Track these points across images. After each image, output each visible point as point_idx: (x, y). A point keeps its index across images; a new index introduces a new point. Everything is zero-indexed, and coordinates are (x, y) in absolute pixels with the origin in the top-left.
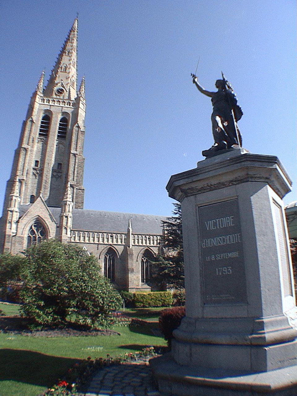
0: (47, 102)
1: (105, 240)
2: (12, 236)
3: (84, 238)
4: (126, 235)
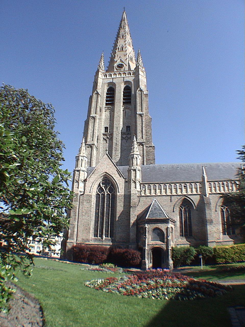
0: (109, 76)
1: (179, 191)
2: (79, 195)
3: (156, 191)
4: (201, 183)
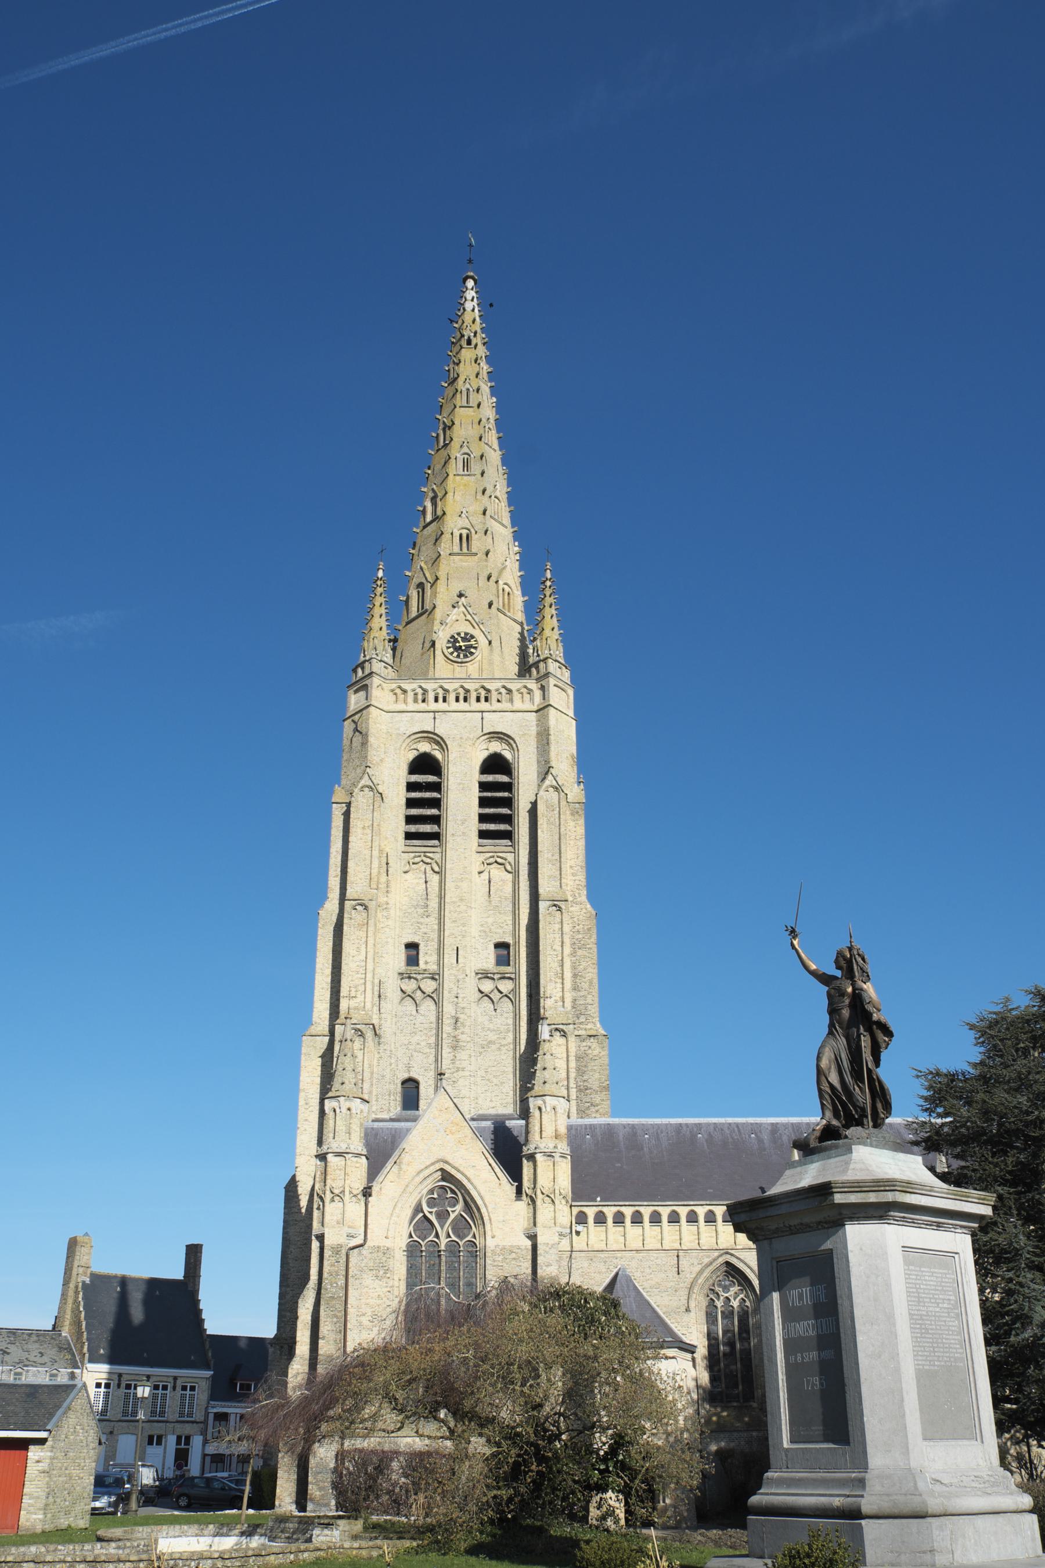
0: (416, 701)
